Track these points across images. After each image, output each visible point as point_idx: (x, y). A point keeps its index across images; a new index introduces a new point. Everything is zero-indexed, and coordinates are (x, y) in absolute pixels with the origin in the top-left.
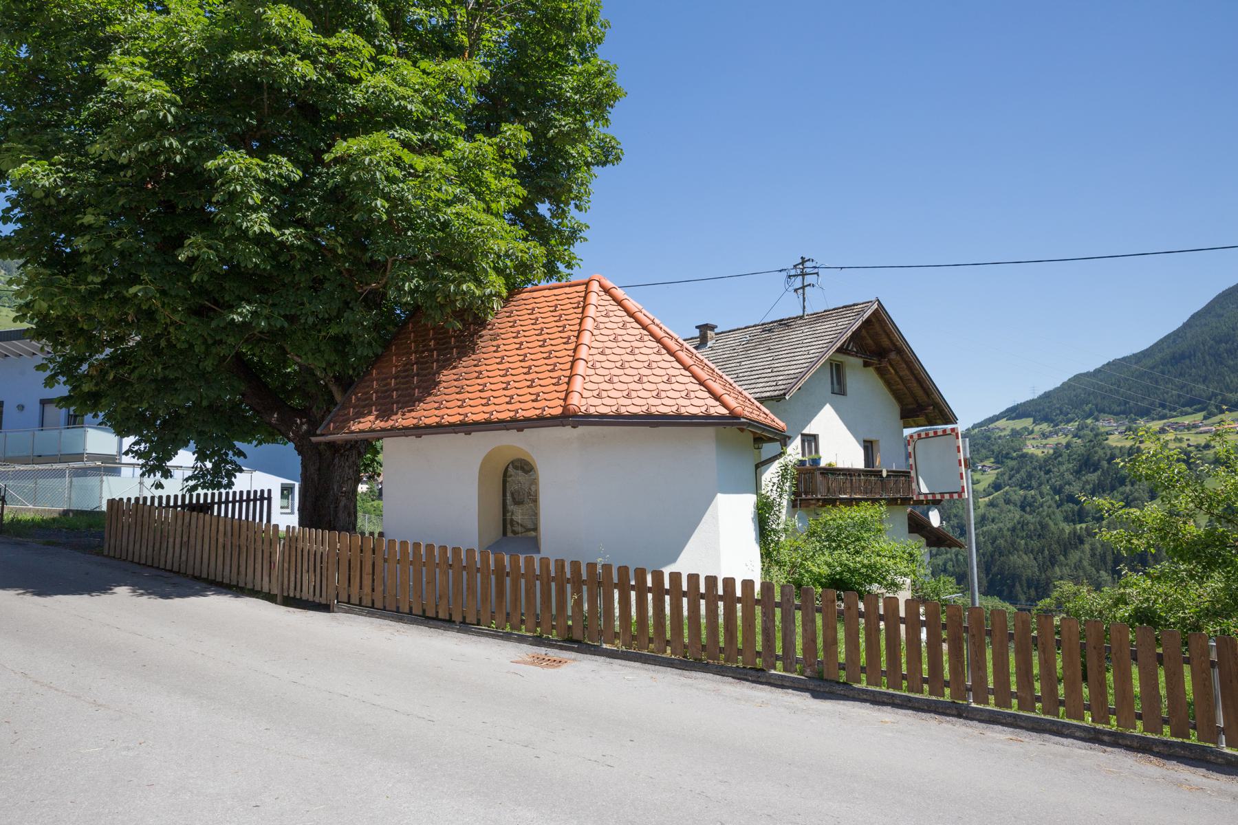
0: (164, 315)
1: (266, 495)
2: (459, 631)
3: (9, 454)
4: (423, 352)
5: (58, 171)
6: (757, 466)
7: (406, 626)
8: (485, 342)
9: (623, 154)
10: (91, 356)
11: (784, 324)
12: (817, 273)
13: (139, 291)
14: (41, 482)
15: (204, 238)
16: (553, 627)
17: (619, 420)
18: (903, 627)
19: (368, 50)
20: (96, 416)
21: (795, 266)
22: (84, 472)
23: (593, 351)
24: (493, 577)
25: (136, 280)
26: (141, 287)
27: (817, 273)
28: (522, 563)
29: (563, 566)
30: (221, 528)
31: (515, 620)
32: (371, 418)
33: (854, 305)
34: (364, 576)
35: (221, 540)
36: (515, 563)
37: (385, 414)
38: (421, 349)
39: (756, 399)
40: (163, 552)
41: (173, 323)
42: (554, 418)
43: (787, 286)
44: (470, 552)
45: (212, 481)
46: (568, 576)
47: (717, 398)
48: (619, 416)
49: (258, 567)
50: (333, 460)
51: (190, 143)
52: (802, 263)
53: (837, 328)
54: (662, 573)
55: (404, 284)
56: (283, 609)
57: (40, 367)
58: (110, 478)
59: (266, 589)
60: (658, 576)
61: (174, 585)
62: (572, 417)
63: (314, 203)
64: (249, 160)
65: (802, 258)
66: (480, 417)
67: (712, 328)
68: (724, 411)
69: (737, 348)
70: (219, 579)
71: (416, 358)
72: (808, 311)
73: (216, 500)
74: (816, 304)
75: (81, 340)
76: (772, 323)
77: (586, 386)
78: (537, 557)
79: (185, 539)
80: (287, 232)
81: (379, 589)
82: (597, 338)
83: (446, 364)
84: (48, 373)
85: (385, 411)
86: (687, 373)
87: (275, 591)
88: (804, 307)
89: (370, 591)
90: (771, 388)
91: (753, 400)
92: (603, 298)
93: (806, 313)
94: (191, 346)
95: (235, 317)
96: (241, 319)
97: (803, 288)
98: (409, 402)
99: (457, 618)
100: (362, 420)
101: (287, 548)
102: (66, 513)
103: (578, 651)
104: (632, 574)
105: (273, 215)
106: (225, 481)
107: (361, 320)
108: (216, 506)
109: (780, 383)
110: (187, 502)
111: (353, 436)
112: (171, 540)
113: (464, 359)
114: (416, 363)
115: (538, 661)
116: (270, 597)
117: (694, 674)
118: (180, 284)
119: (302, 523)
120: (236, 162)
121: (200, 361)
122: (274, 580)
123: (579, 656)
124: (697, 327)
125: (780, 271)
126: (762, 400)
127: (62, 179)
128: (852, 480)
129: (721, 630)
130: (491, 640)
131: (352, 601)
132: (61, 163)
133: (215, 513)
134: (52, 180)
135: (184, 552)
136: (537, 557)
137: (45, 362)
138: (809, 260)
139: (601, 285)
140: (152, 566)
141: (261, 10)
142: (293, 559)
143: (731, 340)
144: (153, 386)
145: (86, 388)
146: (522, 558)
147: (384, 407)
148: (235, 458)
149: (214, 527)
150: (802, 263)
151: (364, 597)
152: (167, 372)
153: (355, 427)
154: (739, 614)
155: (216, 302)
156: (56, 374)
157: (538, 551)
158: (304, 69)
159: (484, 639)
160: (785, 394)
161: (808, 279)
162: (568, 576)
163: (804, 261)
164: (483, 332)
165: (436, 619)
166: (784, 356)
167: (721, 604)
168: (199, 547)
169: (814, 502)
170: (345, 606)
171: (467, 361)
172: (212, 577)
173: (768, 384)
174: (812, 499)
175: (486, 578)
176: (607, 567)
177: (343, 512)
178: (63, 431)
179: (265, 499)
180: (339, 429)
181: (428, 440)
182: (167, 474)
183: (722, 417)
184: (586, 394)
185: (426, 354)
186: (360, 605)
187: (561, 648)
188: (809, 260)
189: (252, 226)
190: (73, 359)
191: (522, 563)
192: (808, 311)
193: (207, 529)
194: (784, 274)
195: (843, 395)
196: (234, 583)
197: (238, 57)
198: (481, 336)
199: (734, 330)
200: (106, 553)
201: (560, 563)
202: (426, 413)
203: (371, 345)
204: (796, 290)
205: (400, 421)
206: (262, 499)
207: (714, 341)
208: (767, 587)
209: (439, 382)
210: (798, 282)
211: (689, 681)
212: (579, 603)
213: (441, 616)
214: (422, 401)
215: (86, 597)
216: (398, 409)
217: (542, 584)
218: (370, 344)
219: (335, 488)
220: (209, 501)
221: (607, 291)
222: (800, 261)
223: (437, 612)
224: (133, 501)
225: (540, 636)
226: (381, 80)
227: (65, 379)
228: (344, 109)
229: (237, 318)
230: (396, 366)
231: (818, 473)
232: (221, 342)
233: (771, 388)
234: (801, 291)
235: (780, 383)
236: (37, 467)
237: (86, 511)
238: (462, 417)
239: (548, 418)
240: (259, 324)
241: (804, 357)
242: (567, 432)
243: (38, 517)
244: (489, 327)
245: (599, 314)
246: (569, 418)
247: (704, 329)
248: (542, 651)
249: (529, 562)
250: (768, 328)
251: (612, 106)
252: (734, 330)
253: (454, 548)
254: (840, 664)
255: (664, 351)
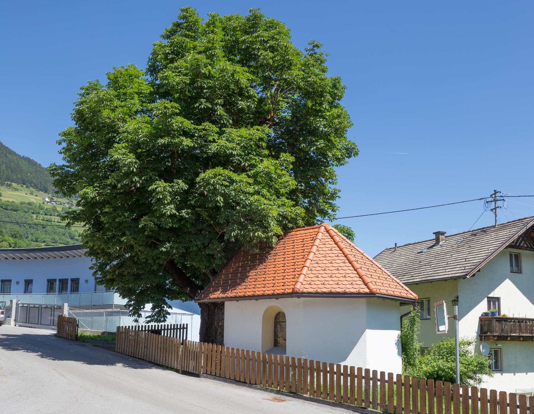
0: (137, 248)
1: (185, 327)
2: (248, 387)
3: (83, 304)
4: (245, 261)
5: (96, 190)
6: (402, 317)
7: (227, 384)
8: (270, 258)
9: (359, 151)
10: (110, 263)
11: (484, 230)
12: (503, 200)
13: (125, 239)
14: (95, 318)
15: (149, 217)
16: (284, 386)
17: (309, 295)
18: (470, 401)
19: (216, 129)
20: (113, 289)
21: (491, 195)
22: (111, 314)
23: (313, 262)
24: (262, 363)
25: (124, 234)
26: (126, 238)
27: (503, 200)
28: (278, 359)
29: (288, 359)
30: (160, 340)
31: (270, 383)
32: (219, 292)
33: (525, 219)
34: (213, 362)
35: (159, 346)
36: (276, 358)
37: (224, 291)
38: (245, 260)
39: (403, 283)
40: (138, 351)
41: (139, 251)
42: (289, 294)
43: (486, 208)
44: (259, 353)
45: (157, 319)
46: (291, 364)
47: (366, 284)
48: (317, 293)
49: (173, 357)
50: (215, 310)
51: (143, 178)
52: (495, 194)
53: (510, 234)
54: (340, 365)
55: (231, 233)
56: (181, 375)
57: (91, 268)
58: (124, 317)
59: (175, 368)
60: (339, 366)
61: (140, 364)
62: (295, 293)
63: (195, 197)
64: (165, 184)
65: (495, 191)
66: (271, 292)
67: (443, 234)
68: (367, 291)
69: (454, 246)
70: (158, 363)
71: (242, 264)
72: (498, 223)
73: (163, 328)
74: (502, 219)
75: (106, 257)
76: (478, 230)
77: (305, 279)
78: (284, 356)
79: (146, 345)
80: (183, 211)
81: (223, 369)
82: (317, 256)
83: (253, 267)
84: (94, 270)
85: (225, 289)
86: (355, 272)
87: (179, 368)
88: (496, 220)
89: (215, 369)
90: (461, 271)
91: (403, 285)
92: (325, 235)
93: (497, 224)
94: (147, 260)
95: (163, 249)
96: (165, 250)
97: (495, 208)
98: (234, 285)
99: (248, 381)
100: (215, 293)
101: (184, 349)
102: (104, 333)
103: (293, 397)
104: (328, 365)
105: (177, 204)
106: (162, 319)
107: (217, 248)
108: (163, 331)
109: (467, 268)
110: (150, 329)
111: (210, 301)
112: (141, 345)
113: (261, 265)
114: (241, 267)
115: (275, 399)
116: (177, 371)
117: (337, 408)
118: (141, 235)
119: (201, 340)
120: (160, 185)
121: (152, 266)
122: (179, 363)
123: (293, 399)
124: (434, 233)
125: (480, 199)
126: (406, 284)
127: (97, 193)
128: (520, 325)
129: (349, 391)
130: (259, 391)
131: (208, 373)
132: (97, 187)
133: (162, 335)
134: (94, 194)
135: (146, 350)
136: (284, 356)
137: (93, 265)
138: (498, 192)
139: (325, 229)
140: (133, 357)
141: (170, 120)
142: (186, 354)
143: (452, 241)
144: (133, 277)
145: (108, 277)
146: (278, 356)
147: (224, 288)
148: (167, 309)
149: (157, 340)
150: (495, 194)
151: (212, 372)
152: (138, 271)
153: (212, 296)
154: (335, 379)
155: (158, 240)
156: (97, 271)
157: (285, 354)
158: (187, 142)
159: (257, 391)
160: (467, 275)
161: (499, 204)
162: (291, 364)
163: (496, 192)
164: (271, 252)
165: (240, 381)
166: (476, 251)
167: (371, 382)
168: (151, 349)
169: (491, 337)
170: (205, 375)
171: (262, 266)
172: (156, 362)
173: (461, 269)
174: (491, 336)
175: (259, 364)
176: (305, 360)
177: (219, 335)
178: (104, 293)
179: (185, 328)
180: (205, 297)
181: (241, 302)
182: (140, 316)
183: (366, 293)
184: (304, 283)
185: (246, 262)
186: (211, 375)
187: (287, 395)
188: (498, 192)
189: (167, 211)
190: (104, 264)
191: (278, 359)
192: (498, 223)
193: (154, 341)
194: (483, 201)
195: (520, 273)
196: (164, 364)
197: (161, 141)
198: (270, 254)
199: (457, 235)
200: (116, 351)
201: (287, 358)
202: (240, 291)
203: (222, 259)
204: (492, 210)
205: (230, 294)
206: (184, 328)
207: (444, 241)
208: (407, 377)
209: (249, 276)
210: (492, 205)
211: (333, 411)
212: (294, 375)
213: (241, 380)
214: (240, 285)
215: (105, 366)
216: (230, 288)
217: (280, 367)
218: (221, 258)
219: (216, 323)
220: (160, 328)
221: (328, 231)
222: (494, 192)
223: (240, 379)
224: (127, 328)
225: (280, 391)
226: (222, 142)
227: (100, 273)
228: (207, 155)
229: (164, 249)
230: (233, 268)
231: (494, 321)
232: (159, 258)
233: (461, 271)
234: (494, 210)
235: (467, 268)
236: (93, 311)
237: (112, 333)
238: (263, 292)
239: (286, 294)
240: (173, 251)
241: (485, 252)
242: (295, 299)
243: (92, 335)
244: (274, 249)
245: (321, 243)
246: (295, 294)
247: (438, 234)
248: (278, 396)
249: (282, 359)
250: (474, 234)
251: (346, 131)
252: (457, 235)
253: (247, 351)
254: (394, 406)
255: (347, 261)
